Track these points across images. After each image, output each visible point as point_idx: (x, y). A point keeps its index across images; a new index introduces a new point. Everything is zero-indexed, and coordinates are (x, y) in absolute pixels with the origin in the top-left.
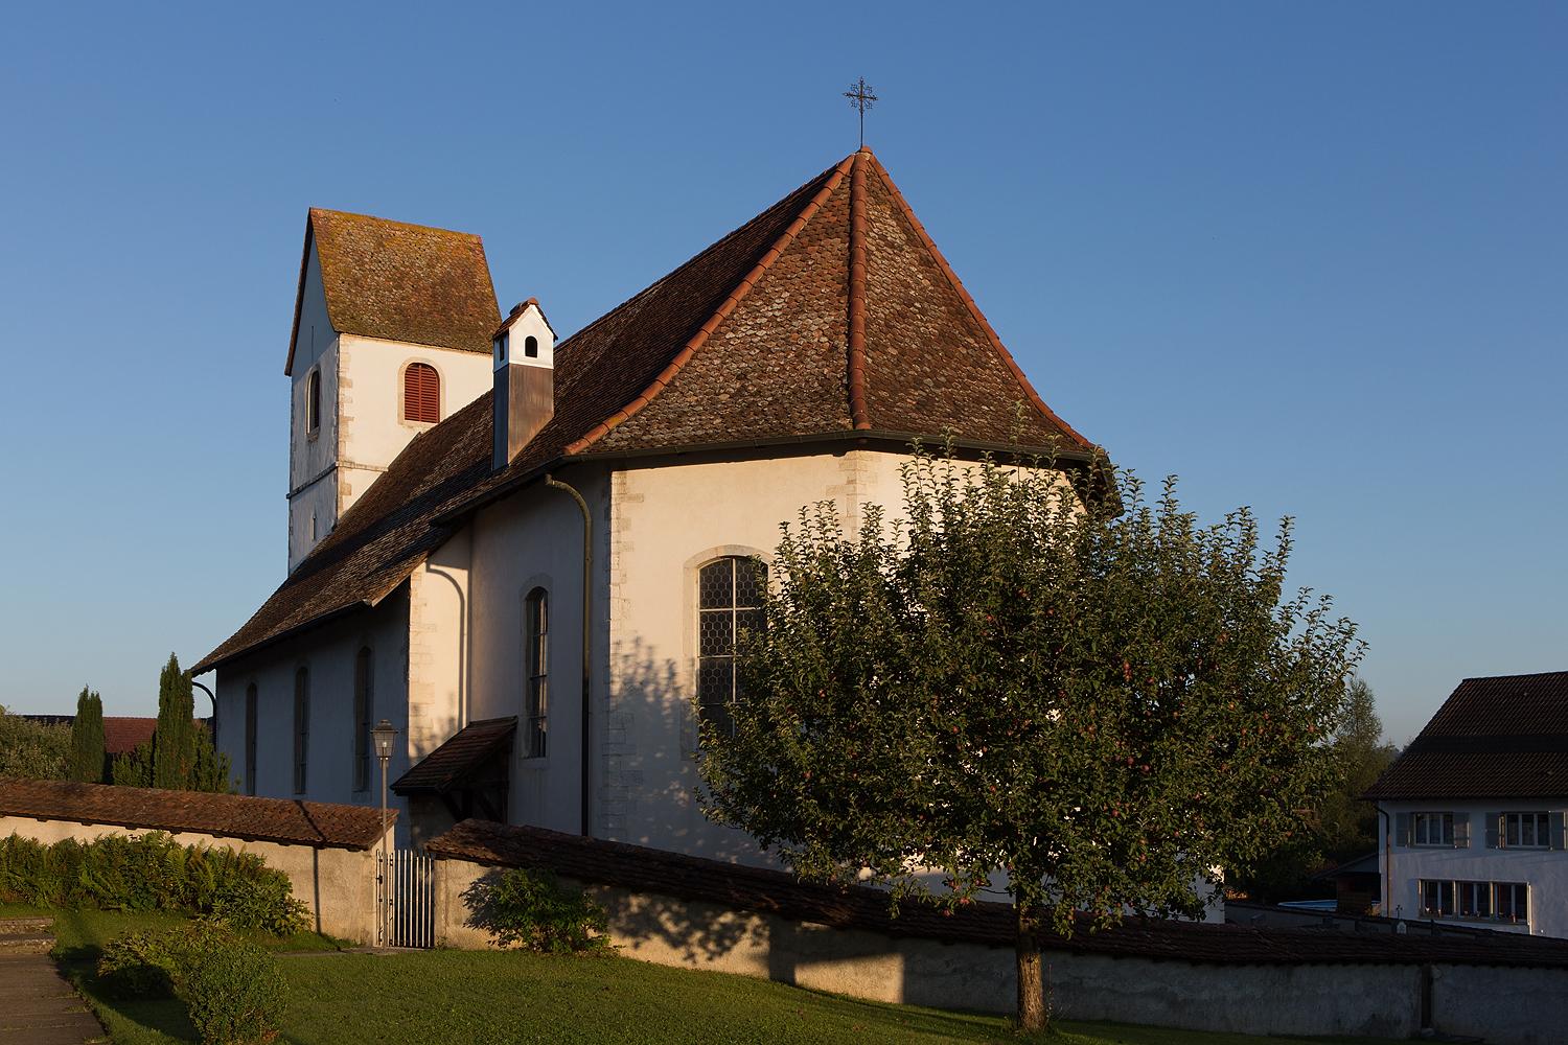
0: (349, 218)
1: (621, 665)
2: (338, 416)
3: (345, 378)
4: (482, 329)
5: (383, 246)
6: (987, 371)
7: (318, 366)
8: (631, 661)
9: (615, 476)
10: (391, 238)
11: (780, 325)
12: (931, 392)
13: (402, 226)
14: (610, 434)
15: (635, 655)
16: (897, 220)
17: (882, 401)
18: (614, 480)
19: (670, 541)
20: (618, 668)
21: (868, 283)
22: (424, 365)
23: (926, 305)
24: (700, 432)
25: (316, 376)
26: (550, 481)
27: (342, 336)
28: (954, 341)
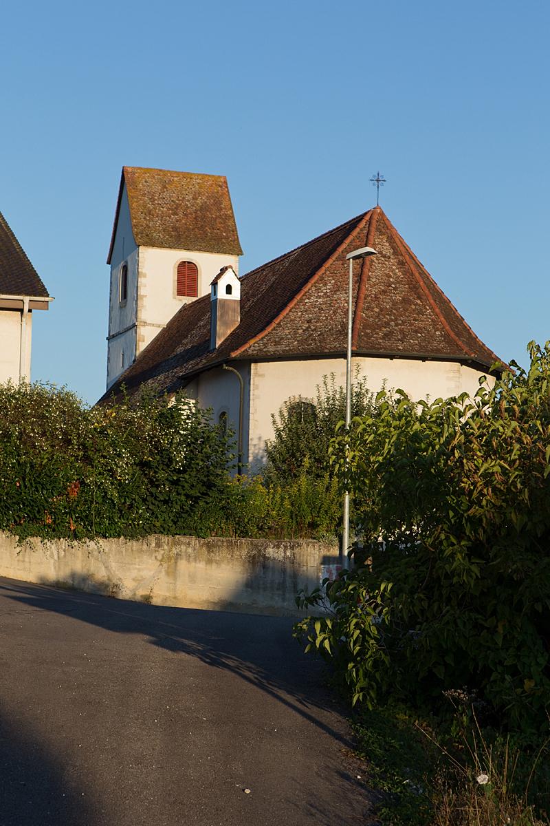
0: (147, 170)
1: (253, 449)
2: (137, 294)
3: (142, 272)
4: (225, 238)
5: (166, 188)
6: (425, 316)
7: (126, 262)
8: (257, 447)
9: (252, 365)
10: (171, 182)
11: (328, 296)
12: (393, 329)
13: (178, 173)
14: (250, 347)
15: (258, 444)
16: (390, 243)
17: (367, 335)
18: (252, 367)
19: (276, 391)
20: (252, 450)
21: (369, 277)
22: (189, 262)
23: (398, 285)
24: (287, 348)
25: (125, 268)
26: (225, 367)
27: (140, 247)
28: (410, 302)
